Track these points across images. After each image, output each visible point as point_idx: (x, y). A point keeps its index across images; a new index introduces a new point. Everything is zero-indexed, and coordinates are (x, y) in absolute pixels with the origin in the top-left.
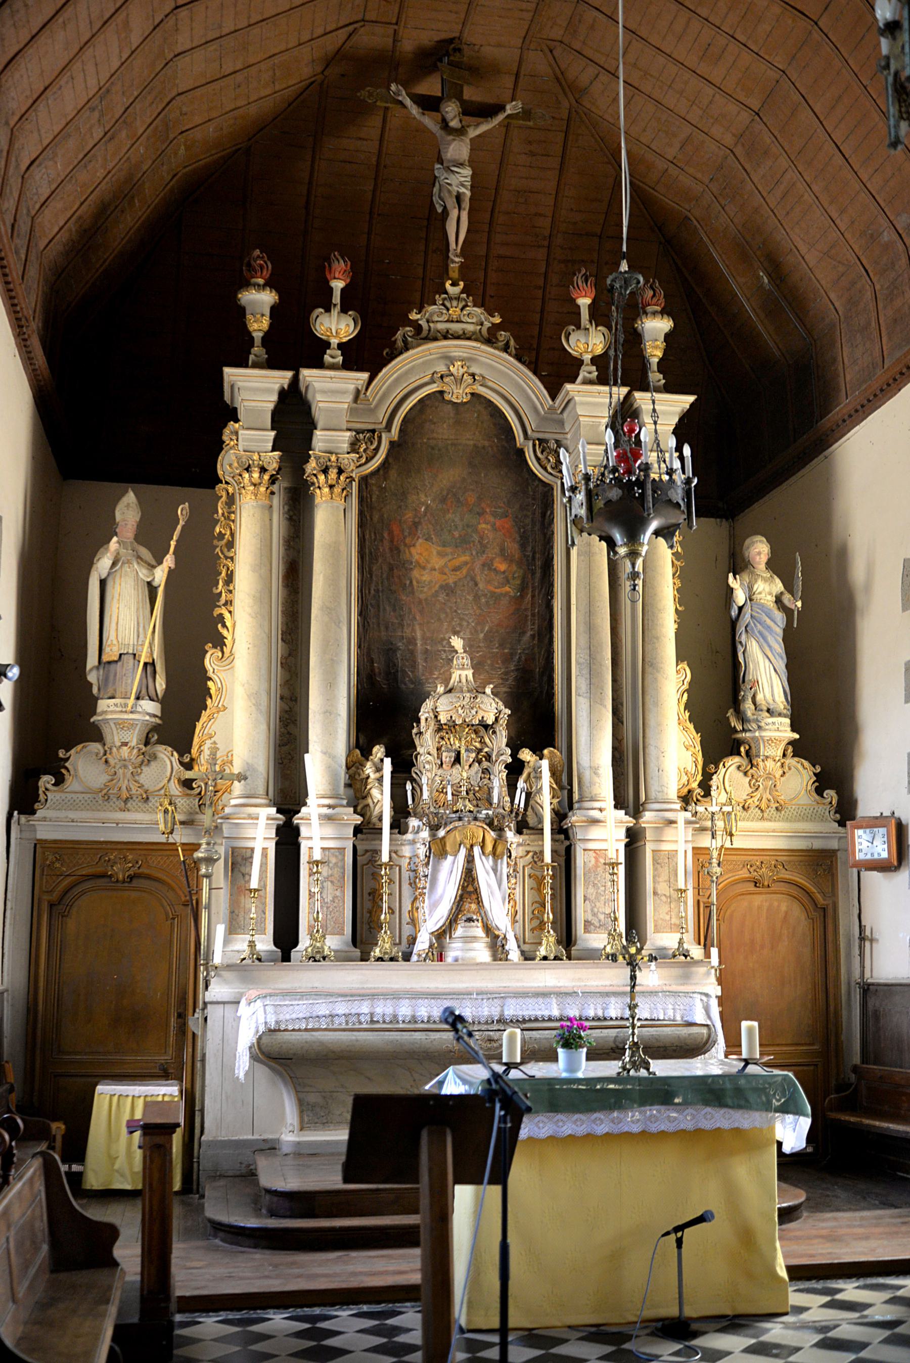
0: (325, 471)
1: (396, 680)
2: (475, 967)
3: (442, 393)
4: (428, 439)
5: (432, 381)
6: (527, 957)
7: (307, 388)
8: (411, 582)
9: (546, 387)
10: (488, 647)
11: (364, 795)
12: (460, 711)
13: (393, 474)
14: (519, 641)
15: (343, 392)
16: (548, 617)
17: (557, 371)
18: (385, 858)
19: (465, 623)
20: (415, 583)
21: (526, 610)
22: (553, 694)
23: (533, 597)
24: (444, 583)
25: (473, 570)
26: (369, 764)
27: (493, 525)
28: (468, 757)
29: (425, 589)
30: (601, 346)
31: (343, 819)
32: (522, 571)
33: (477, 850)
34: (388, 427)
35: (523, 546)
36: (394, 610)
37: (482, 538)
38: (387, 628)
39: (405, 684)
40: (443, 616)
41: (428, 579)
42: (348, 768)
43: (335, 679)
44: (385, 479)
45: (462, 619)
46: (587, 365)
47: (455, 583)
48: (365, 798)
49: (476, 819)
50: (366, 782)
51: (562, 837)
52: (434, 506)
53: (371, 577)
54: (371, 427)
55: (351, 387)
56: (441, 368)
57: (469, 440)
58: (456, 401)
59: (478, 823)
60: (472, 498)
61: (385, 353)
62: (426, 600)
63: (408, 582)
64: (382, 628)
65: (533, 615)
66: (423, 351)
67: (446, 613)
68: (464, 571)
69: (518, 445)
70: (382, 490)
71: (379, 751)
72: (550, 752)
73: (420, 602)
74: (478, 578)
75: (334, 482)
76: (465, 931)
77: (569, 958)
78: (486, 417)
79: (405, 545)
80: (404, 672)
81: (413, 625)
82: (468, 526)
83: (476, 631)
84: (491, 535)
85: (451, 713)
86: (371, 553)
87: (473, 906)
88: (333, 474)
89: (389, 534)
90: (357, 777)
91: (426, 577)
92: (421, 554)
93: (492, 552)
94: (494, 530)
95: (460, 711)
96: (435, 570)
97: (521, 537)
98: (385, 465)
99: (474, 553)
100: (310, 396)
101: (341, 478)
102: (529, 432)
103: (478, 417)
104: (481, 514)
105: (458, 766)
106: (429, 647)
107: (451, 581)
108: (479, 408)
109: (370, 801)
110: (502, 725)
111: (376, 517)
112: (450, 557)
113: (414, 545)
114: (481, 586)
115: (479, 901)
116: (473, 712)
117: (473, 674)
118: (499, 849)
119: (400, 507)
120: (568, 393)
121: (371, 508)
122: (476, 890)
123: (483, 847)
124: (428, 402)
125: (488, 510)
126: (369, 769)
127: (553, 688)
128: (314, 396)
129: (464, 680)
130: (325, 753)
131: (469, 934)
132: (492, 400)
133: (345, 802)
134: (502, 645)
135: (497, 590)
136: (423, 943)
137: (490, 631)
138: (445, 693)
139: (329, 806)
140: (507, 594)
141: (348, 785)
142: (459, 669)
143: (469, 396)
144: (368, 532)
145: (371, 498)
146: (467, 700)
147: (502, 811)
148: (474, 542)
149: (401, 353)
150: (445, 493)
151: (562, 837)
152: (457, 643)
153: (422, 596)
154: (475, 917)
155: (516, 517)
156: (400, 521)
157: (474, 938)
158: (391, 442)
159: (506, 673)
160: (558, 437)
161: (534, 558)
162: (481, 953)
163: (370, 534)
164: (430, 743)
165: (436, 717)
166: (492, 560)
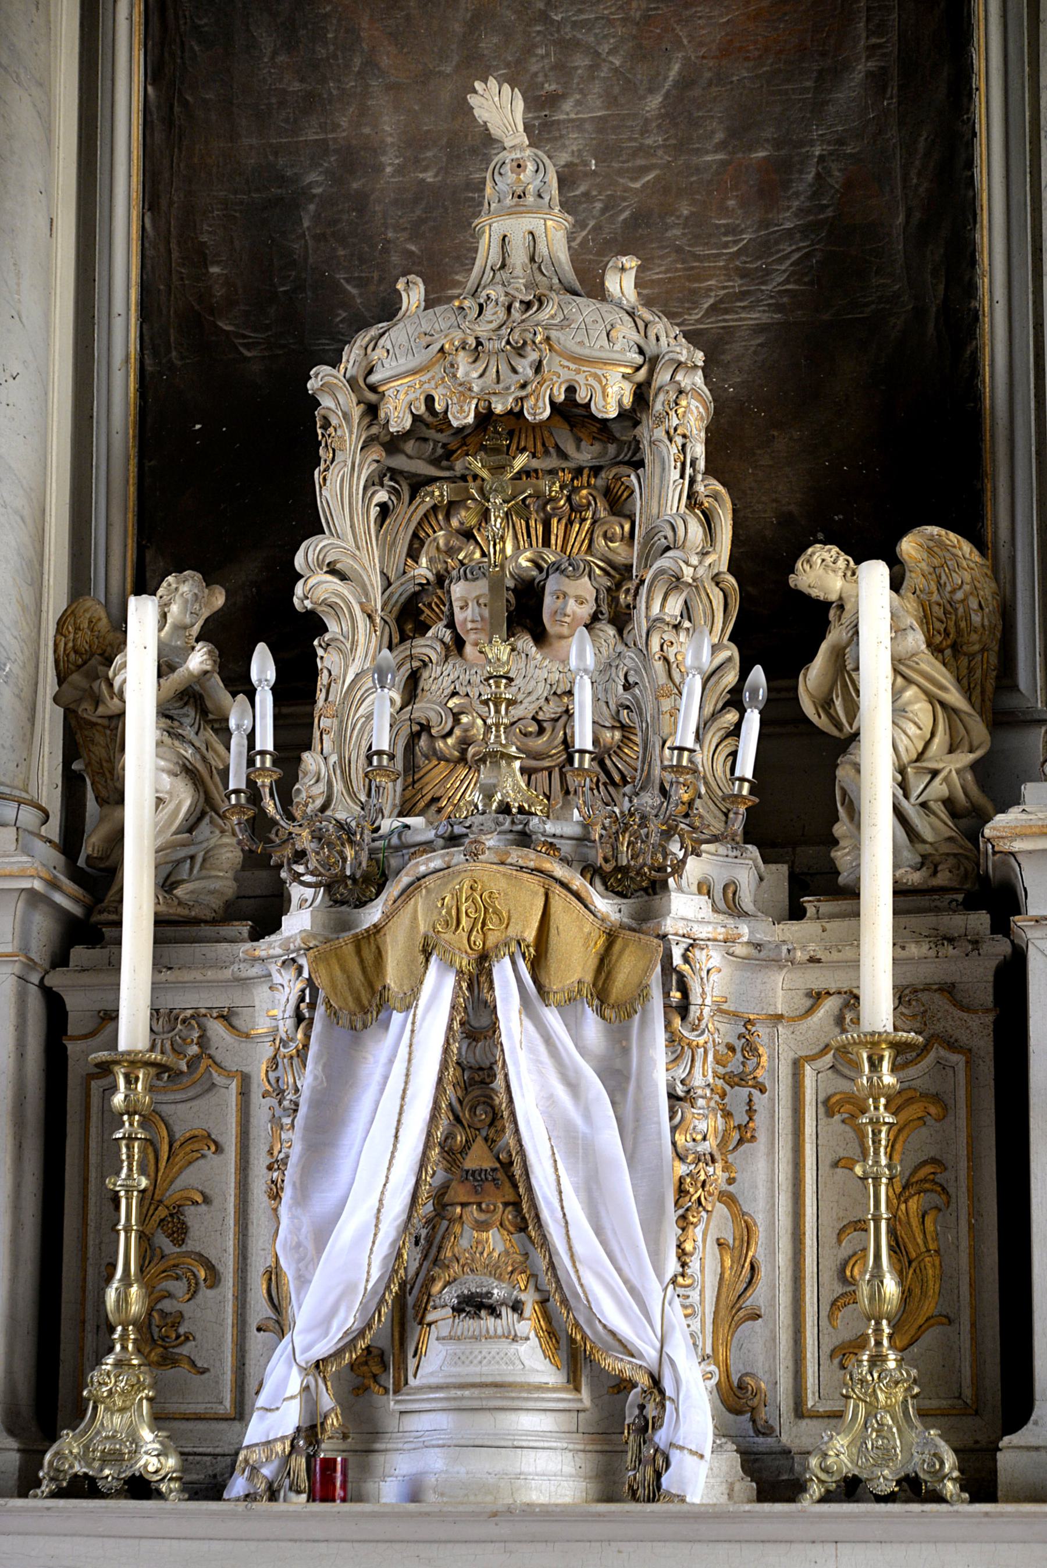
2: (491, 1529)
6: (772, 1476)
10: (680, 147)
18: (132, 1031)
22: (975, 317)
33: (507, 982)
45: (574, 45)
49: (524, 839)
51: (980, 920)
59: (530, 858)
72: (932, 548)
76: (458, 1359)
77: (981, 1486)
87: (496, 1242)
115: (524, 1218)
118: (626, 969)
122: (507, 1166)
123: (538, 962)
127: (971, 290)
129: (519, 257)
131: (473, 1372)
134: (740, 133)
136: (277, 1414)
137: (685, 83)
146: (494, 314)
151: (980, 920)
154: (498, 1293)
157: (503, 1393)
159: (764, 248)
162: (548, 1466)
165: (372, 411)
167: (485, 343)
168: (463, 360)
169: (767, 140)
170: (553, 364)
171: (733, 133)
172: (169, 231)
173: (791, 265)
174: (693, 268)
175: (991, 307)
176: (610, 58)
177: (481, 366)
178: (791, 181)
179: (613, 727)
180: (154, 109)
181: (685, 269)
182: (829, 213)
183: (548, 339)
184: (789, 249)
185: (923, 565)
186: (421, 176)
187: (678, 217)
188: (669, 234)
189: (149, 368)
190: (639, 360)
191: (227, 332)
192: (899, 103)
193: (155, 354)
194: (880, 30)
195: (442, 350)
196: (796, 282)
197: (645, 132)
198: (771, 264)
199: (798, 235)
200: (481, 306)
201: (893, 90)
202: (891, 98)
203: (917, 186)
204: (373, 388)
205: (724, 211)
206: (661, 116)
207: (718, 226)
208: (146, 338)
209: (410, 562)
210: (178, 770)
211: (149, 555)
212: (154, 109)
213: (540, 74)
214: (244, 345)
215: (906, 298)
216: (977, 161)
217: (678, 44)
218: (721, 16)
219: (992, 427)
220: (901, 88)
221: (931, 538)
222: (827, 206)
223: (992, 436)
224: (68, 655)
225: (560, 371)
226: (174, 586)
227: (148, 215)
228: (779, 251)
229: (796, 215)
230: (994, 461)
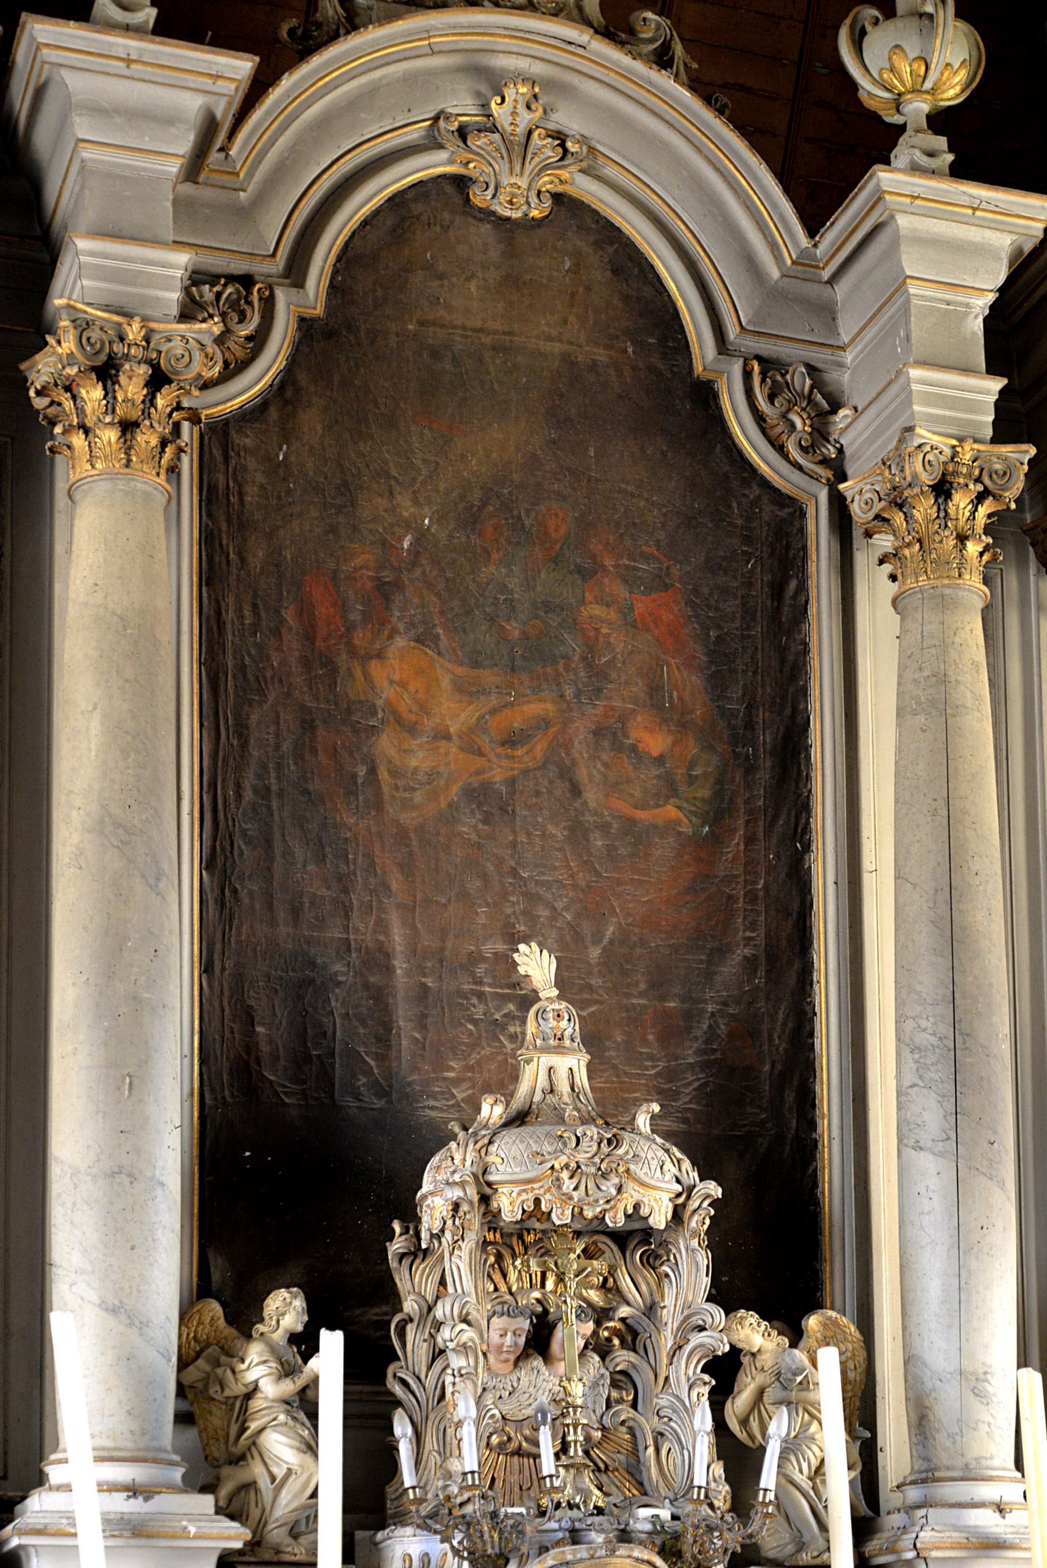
0: (106, 372)
1: (327, 1078)
3: (461, 183)
4: (421, 323)
5: (432, 143)
7: (40, 92)
8: (373, 771)
9: (787, 191)
11: (237, 1450)
12: (568, 1185)
13: (311, 421)
14: (709, 976)
15: (167, 120)
16: (795, 906)
17: (825, 151)
19: (543, 912)
20: (383, 774)
21: (729, 879)
23: (750, 840)
24: (475, 781)
25: (567, 746)
26: (255, 1352)
27: (626, 611)
28: (573, 1333)
29: (418, 797)
30: (962, 76)
31: (184, 1534)
32: (715, 760)
34: (296, 271)
35: (717, 683)
36: (321, 860)
37: (591, 648)
38: (296, 913)
39: (357, 1097)
40: (474, 884)
41: (426, 766)
42: (183, 1364)
43: (145, 1062)
44: (286, 437)
45: (533, 898)
46: (918, 131)
47: (512, 782)
48: (239, 1459)
49: (625, 1536)
50: (244, 1408)
52: (443, 535)
53: (244, 746)
54: (239, 266)
55: (193, 104)
56: (462, 106)
57: (550, 338)
58: (507, 213)
60: (560, 521)
61: (284, 34)
62: (420, 829)
63: (362, 771)
64: (281, 913)
65: (752, 897)
66: (410, 36)
67: (484, 877)
68: (540, 747)
69: (698, 368)
70: (278, 471)
71: (285, 1309)
73: (402, 835)
74: (582, 774)
75: (135, 414)
78: (598, 274)
79: (353, 652)
80: (351, 1054)
81: (382, 909)
82: (548, 607)
83: (578, 938)
84: (619, 641)
85: (538, 1189)
86: (242, 668)
88: (132, 386)
89: (300, 613)
90: (214, 1390)
91: (419, 760)
92: (403, 685)
93: (625, 691)
94: (632, 626)
95: (568, 1185)
96: (448, 737)
97: (710, 653)
98: (284, 391)
99: (569, 692)
100: (42, 139)
101: (160, 402)
102: (732, 332)
103: (576, 269)
104: (587, 573)
105: (538, 1362)
106: (429, 982)
107: (498, 775)
108: (581, 243)
109: (257, 1470)
110: (695, 1234)
111: (258, 555)
112: (494, 701)
113: (380, 656)
114: (592, 796)
116: (609, 1187)
117: (589, 1066)
119: (333, 529)
120: (878, 198)
121: (242, 525)
124: (418, 208)
125: (609, 562)
126: (257, 1368)
127: (812, 1125)
128: (63, 124)
129: (564, 1087)
130: (114, 1311)
132: (618, 221)
133: (177, 1474)
134: (658, 986)
135: (641, 815)
138: (508, 1124)
139: (133, 1490)
140: (671, 826)
141: (183, 1419)
142: (547, 1050)
143: (548, 203)
144: (231, 600)
145: (241, 495)
146: (589, 1147)
147: (705, 1510)
148: (566, 657)
149: (333, 37)
150: (476, 497)
152: (537, 965)
153: (408, 818)
155: (696, 592)
156: (335, 573)
158: (302, 320)
160: (815, 356)
161: (749, 724)
163: (240, 609)
164: (468, 1284)
165: (485, 1199)
166: (624, 719)
167: (583, 1167)
168: (565, 1175)
169: (675, 995)
170: (631, 1187)
171: (652, 985)
172: (222, 992)
173: (694, 1090)
174: (625, 1082)
175: (829, 1141)
176: (564, 913)
177: (575, 1181)
178: (692, 1027)
179: (598, 1429)
180: (208, 890)
181: (618, 1082)
182: (718, 1055)
183: (628, 1171)
184: (692, 1079)
185: (819, 1335)
186: (423, 980)
187: (614, 1042)
188: (607, 1054)
189: (208, 1102)
190: (679, 1188)
191: (271, 1082)
192: (766, 983)
193: (212, 1090)
194: (753, 926)
195: (552, 1168)
196: (697, 1103)
197: (590, 974)
198: (679, 1087)
199: (697, 1069)
200: (578, 1138)
201: (761, 972)
202: (760, 978)
203: (779, 1045)
204: (489, 1184)
205: (645, 1042)
206: (600, 964)
207: (641, 1053)
208: (205, 1077)
209: (441, 1288)
210: (303, 1447)
211: (211, 1254)
212: (208, 890)
213: (513, 917)
214: (285, 1093)
215: (770, 1125)
216: (817, 1033)
217: (613, 912)
218: (643, 896)
219: (830, 1227)
220: (767, 971)
221: (830, 1318)
222: (715, 1050)
223: (830, 1233)
224: (189, 1343)
225: (634, 1193)
226: (288, 1300)
227: (204, 976)
228: (685, 1079)
229: (695, 1053)
230: (831, 1251)
